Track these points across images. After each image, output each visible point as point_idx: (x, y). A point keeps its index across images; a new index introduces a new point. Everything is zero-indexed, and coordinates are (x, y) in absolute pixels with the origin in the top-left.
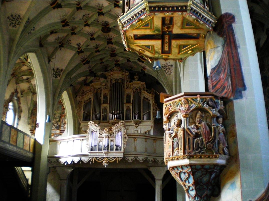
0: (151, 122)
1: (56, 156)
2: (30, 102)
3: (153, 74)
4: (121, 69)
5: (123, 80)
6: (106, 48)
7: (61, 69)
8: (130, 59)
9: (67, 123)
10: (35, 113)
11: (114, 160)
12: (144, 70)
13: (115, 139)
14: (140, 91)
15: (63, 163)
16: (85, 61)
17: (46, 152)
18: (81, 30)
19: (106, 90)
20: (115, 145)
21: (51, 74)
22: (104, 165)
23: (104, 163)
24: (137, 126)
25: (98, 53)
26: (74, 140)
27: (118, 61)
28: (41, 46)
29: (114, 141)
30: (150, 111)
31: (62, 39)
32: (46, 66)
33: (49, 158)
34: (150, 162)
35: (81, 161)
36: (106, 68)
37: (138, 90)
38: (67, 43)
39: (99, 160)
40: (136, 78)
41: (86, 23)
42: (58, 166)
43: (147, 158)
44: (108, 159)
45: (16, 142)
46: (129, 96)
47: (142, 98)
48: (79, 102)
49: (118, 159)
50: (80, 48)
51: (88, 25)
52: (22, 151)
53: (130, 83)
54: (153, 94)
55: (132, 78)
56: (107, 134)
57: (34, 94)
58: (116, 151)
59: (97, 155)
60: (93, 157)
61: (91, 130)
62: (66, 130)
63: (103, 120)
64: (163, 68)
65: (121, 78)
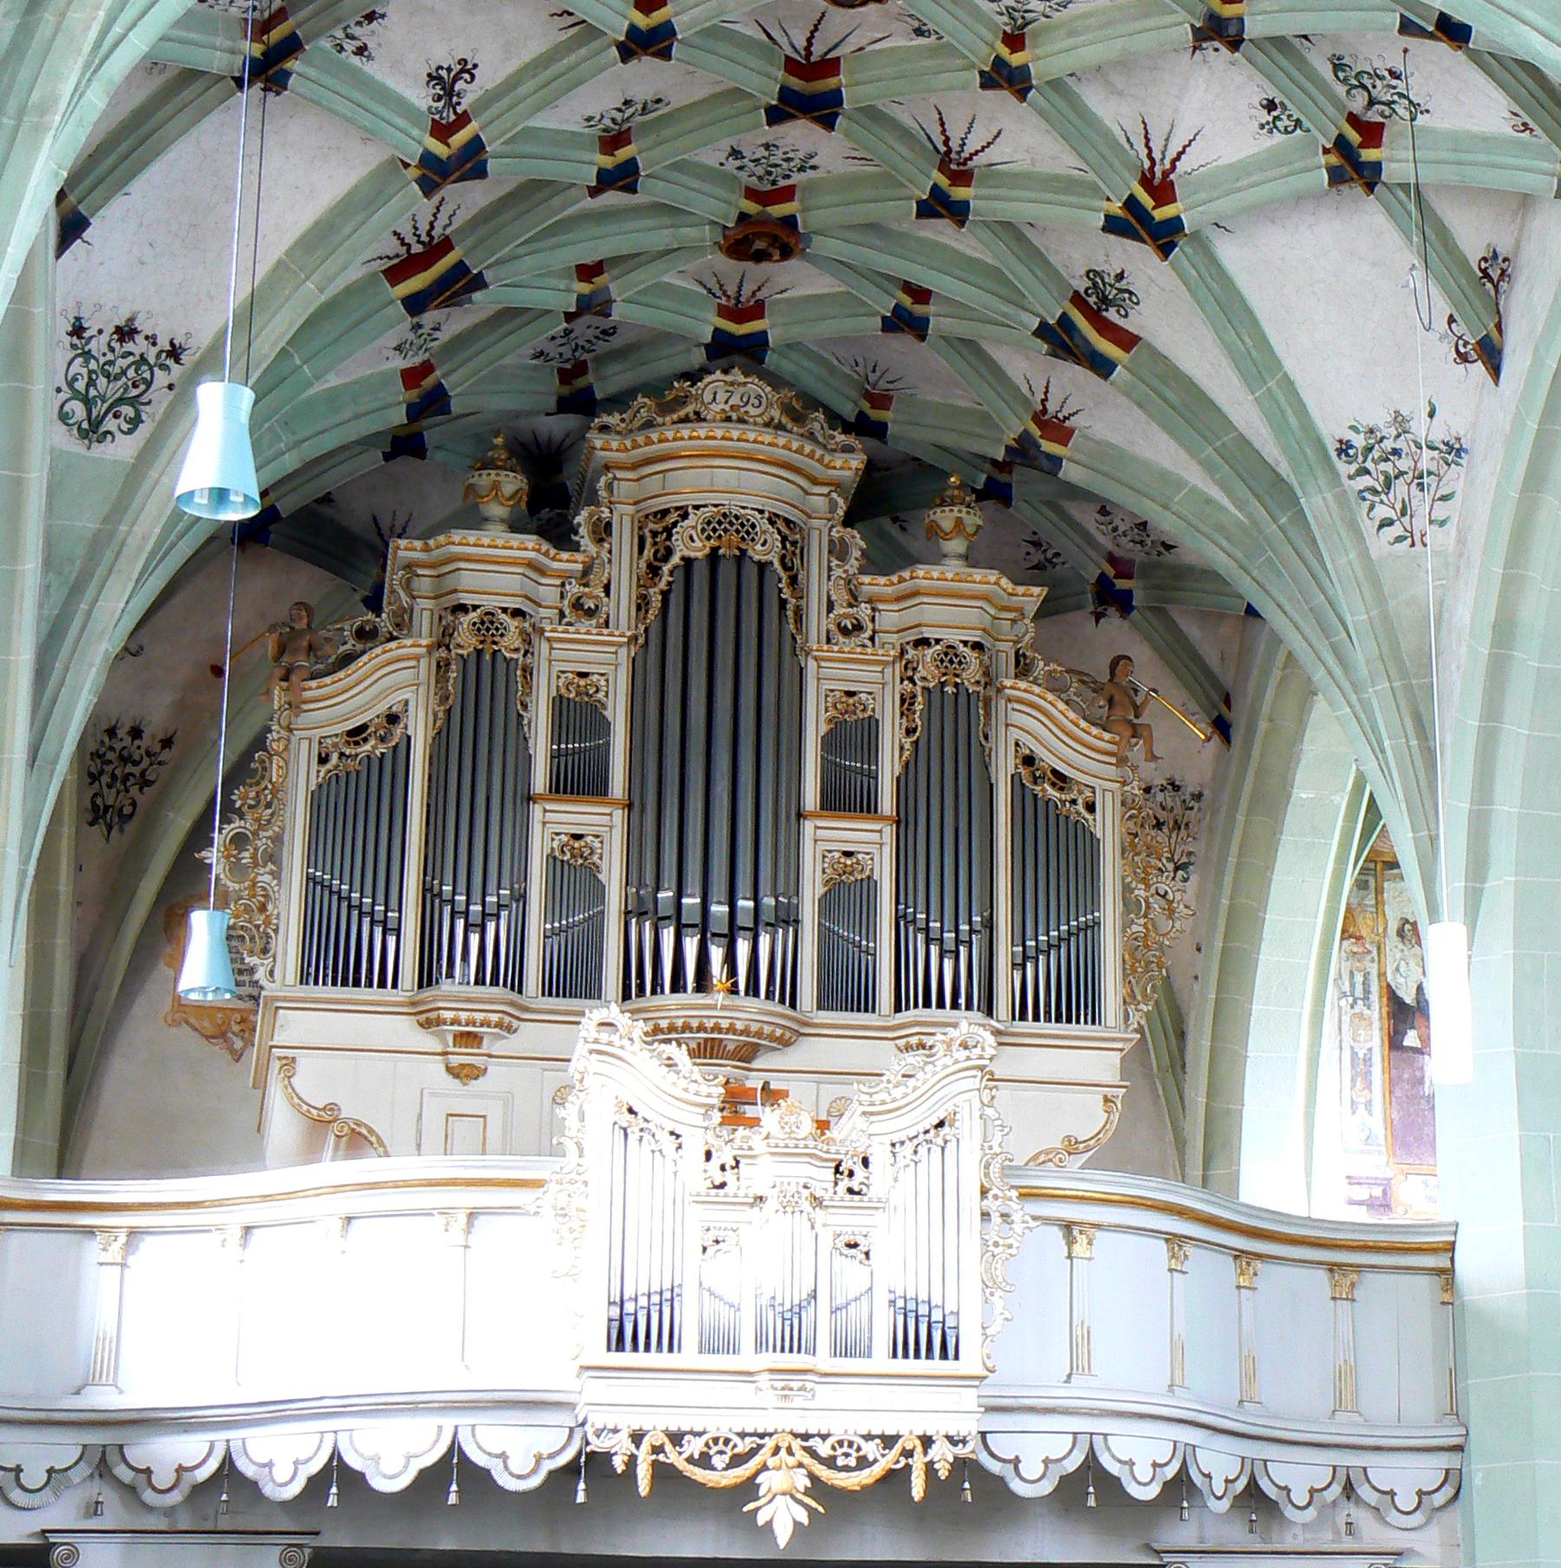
4: (787, 409)
5: (791, 532)
7: (164, 344)
14: (989, 678)
22: (762, 1519)
26: (248, 1230)
27: (757, 311)
34: (1213, 1504)
36: (580, 368)
37: (971, 674)
39: (704, 1461)
40: (959, 522)
46: (853, 737)
47: (1004, 768)
50: (463, 120)
53: (873, 584)
63: (548, 990)
64: (1344, 468)
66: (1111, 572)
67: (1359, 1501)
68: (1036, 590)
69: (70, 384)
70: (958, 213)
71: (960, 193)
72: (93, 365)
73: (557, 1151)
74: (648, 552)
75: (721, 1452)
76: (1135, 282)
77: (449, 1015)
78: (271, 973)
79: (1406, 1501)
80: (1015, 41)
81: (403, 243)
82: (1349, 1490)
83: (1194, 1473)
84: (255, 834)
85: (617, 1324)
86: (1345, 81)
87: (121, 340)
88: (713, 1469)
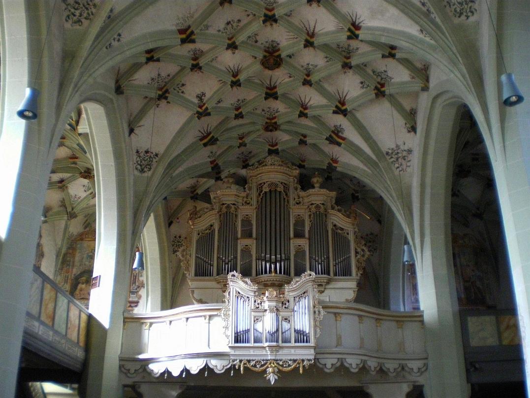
0: (351, 280)
1: (141, 357)
2: (61, 234)
3: (357, 173)
5: (286, 187)
6: (256, 109)
8: (305, 139)
9: (147, 286)
10: (70, 262)
11: (292, 367)
12: (335, 165)
13: (293, 317)
14: (326, 210)
15: (158, 375)
16: (208, 139)
17: (114, 349)
18: (211, 61)
19: (247, 207)
20: (295, 331)
21: (131, 163)
23: (270, 373)
24: (323, 289)
25: (240, 121)
27: (276, 144)
28: (119, 90)
29: (292, 319)
30: (349, 257)
31: (167, 80)
32: (125, 141)
33: (123, 363)
35: (206, 368)
36: (247, 160)
37: (322, 210)
38: (176, 91)
39: (255, 366)
40: (317, 181)
41: (230, 42)
42: (144, 382)
43: (364, 362)
44: (278, 364)
45: (53, 319)
46: (300, 223)
48: (175, 237)
49: (303, 363)
50: (204, 104)
51: (233, 46)
52: (63, 341)
53: (302, 194)
54: (355, 219)
55: (305, 183)
56: (274, 304)
57: (74, 218)
58: (297, 344)
59: (252, 353)
60: (241, 358)
61: (233, 294)
62: (142, 302)
64: (388, 157)
65: (281, 181)
66: (354, 192)
67: (406, 371)
68: (334, 193)
69: (137, 162)
70: (306, 115)
71: (306, 111)
72: (141, 158)
73: (224, 302)
74: (259, 191)
75: (259, 364)
76: (343, 127)
77: (221, 281)
78: (189, 274)
79: (415, 370)
80: (308, 75)
81: (202, 133)
82: (403, 368)
83: (366, 366)
84: (186, 249)
85: (236, 338)
86: (376, 75)
87: (146, 153)
88: (257, 368)
